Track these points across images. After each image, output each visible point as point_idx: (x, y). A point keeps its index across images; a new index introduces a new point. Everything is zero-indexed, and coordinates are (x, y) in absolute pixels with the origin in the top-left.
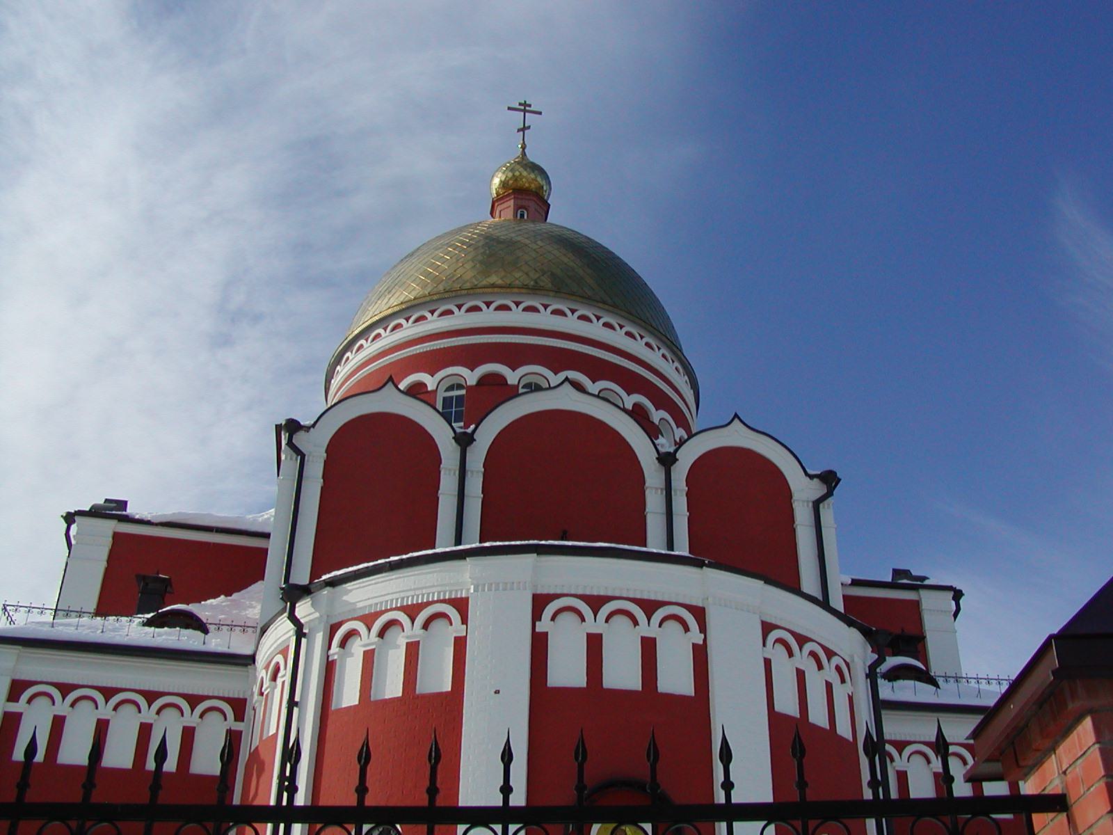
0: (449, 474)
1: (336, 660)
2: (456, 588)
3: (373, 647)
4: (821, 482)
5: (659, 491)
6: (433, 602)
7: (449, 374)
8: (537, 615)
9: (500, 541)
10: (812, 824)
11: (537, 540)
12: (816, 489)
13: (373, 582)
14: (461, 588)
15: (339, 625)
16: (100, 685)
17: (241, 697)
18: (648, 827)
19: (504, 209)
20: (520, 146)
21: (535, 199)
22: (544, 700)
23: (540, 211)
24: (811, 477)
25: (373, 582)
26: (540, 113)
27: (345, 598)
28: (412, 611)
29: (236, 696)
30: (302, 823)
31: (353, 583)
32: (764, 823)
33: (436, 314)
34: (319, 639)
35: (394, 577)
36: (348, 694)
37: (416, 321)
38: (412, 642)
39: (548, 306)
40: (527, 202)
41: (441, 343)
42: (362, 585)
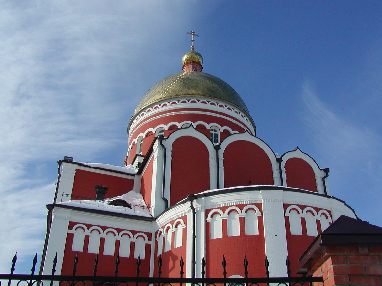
0: (213, 159)
1: (210, 222)
2: (256, 200)
3: (226, 218)
4: (324, 172)
5: (277, 170)
6: (248, 204)
7: (185, 123)
8: (285, 211)
9: (265, 185)
10: (161, 284)
11: (258, 185)
12: (323, 174)
13: (223, 196)
14: (258, 200)
15: (210, 210)
16: (100, 225)
17: (150, 232)
18: (288, 284)
19: (188, 68)
20: (192, 46)
21: (199, 66)
22: (291, 239)
23: (200, 69)
24: (321, 170)
25: (223, 196)
26: (198, 36)
27: (211, 201)
28: (241, 207)
29: (148, 232)
30: (186, 278)
31: (214, 196)
32: (279, 283)
33: (180, 102)
34: (203, 215)
35: (232, 195)
36: (217, 233)
37: (172, 104)
38: (242, 217)
39: (189, 100)
40: (197, 66)
41: (184, 112)
42: (218, 197)
